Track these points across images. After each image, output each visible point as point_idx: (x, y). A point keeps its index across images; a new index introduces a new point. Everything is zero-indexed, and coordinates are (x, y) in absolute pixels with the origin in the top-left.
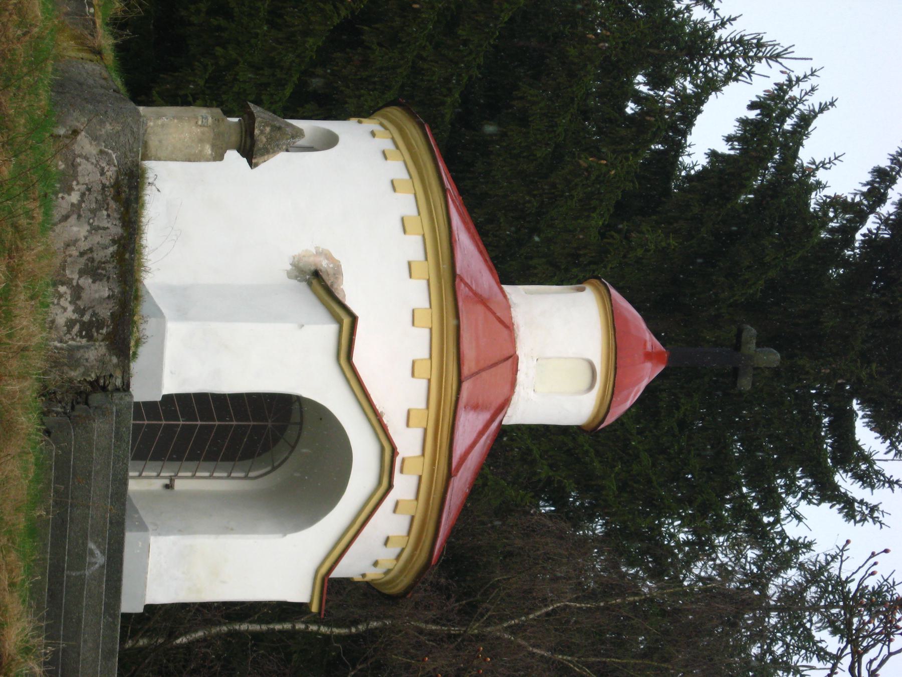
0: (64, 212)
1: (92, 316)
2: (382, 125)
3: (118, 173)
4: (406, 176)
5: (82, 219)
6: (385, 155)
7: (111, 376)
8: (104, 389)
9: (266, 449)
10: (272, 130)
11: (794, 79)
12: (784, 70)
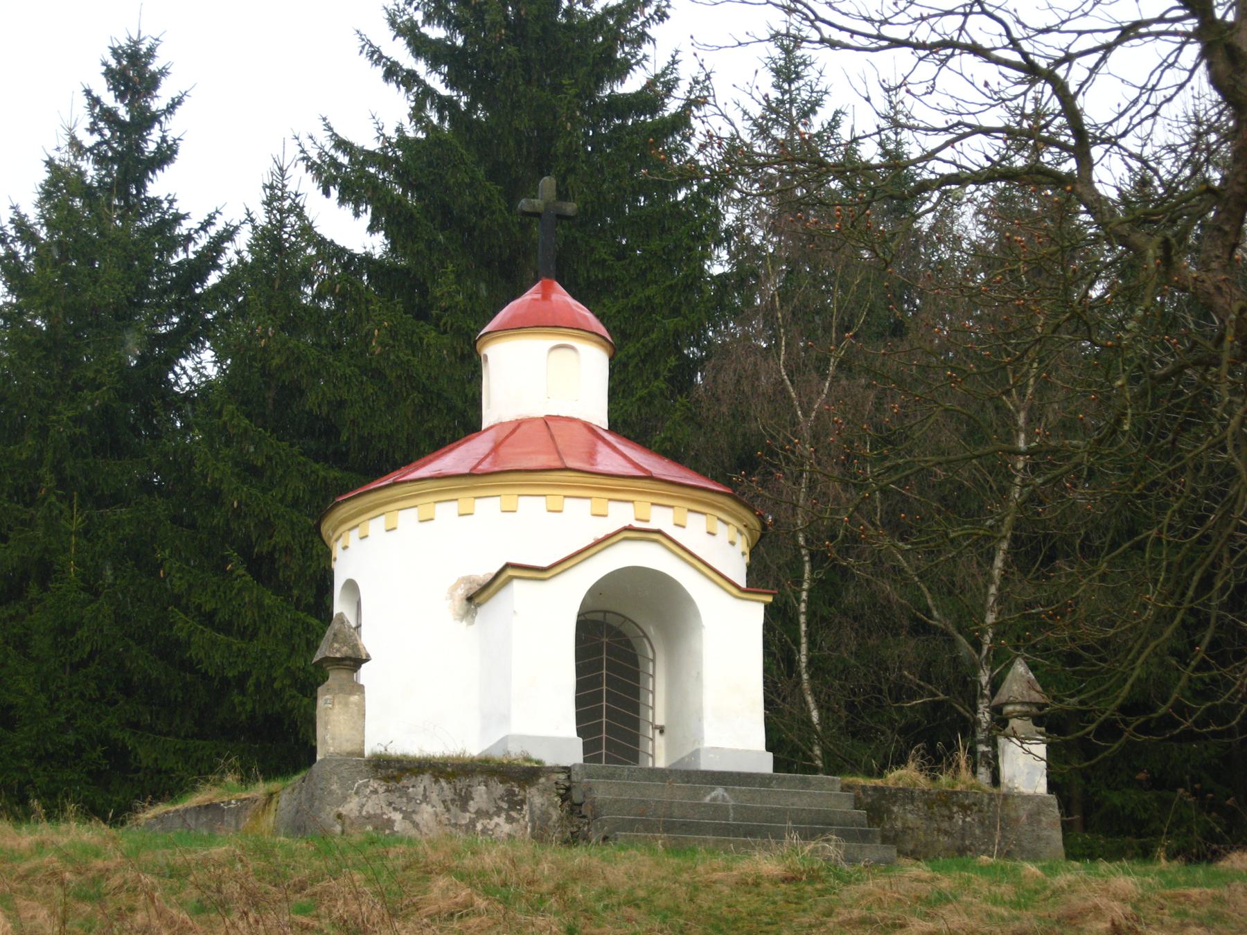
0: (411, 825)
1: (503, 800)
2: (337, 540)
3: (375, 778)
4: (382, 518)
5: (417, 809)
6: (363, 538)
7: (556, 783)
8: (568, 789)
9: (628, 644)
10: (337, 642)
11: (302, 155)
12: (293, 164)
